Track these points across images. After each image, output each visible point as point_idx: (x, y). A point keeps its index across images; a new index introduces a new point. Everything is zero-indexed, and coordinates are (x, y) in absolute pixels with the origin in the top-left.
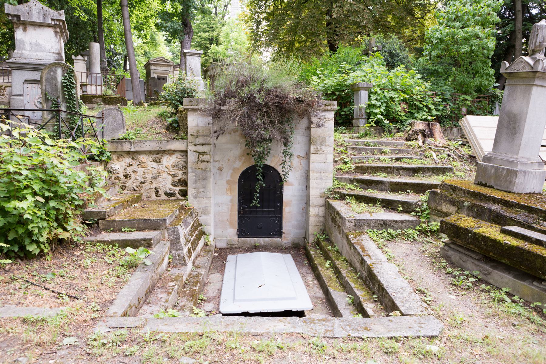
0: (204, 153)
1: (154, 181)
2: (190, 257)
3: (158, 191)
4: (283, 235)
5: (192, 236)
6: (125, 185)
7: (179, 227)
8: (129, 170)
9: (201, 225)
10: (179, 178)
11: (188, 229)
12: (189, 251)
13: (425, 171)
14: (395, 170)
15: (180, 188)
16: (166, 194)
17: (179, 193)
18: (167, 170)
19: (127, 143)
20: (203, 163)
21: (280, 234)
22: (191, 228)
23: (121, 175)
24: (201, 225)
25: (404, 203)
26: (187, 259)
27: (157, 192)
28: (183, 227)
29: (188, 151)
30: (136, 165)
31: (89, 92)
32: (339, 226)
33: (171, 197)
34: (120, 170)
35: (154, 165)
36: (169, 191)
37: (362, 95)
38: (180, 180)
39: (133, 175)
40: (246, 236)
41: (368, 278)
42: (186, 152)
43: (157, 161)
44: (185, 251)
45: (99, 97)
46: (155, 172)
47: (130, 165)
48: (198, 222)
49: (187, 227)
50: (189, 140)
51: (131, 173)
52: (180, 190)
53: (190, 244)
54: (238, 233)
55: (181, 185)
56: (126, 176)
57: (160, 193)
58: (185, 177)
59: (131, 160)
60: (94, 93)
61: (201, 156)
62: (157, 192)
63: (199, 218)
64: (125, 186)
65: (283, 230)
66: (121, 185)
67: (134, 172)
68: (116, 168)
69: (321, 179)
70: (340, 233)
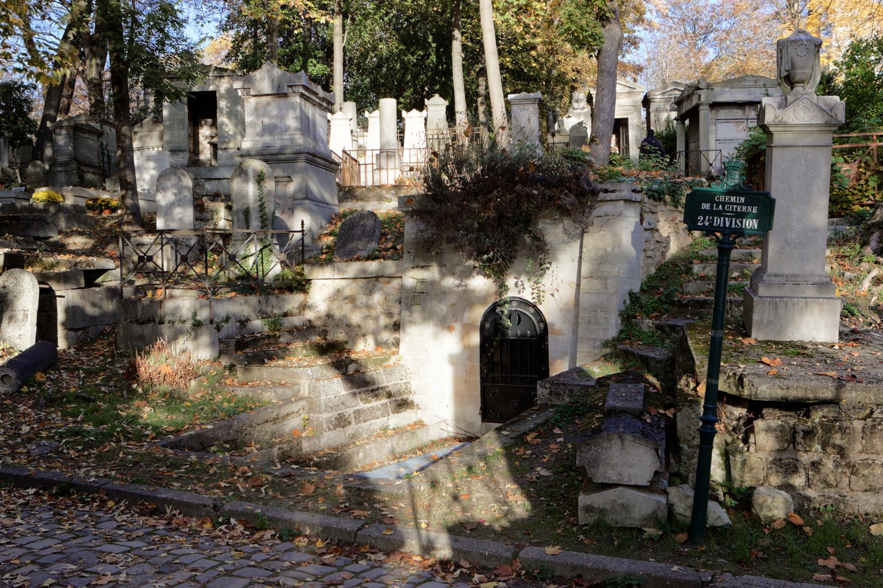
69: (597, 323)
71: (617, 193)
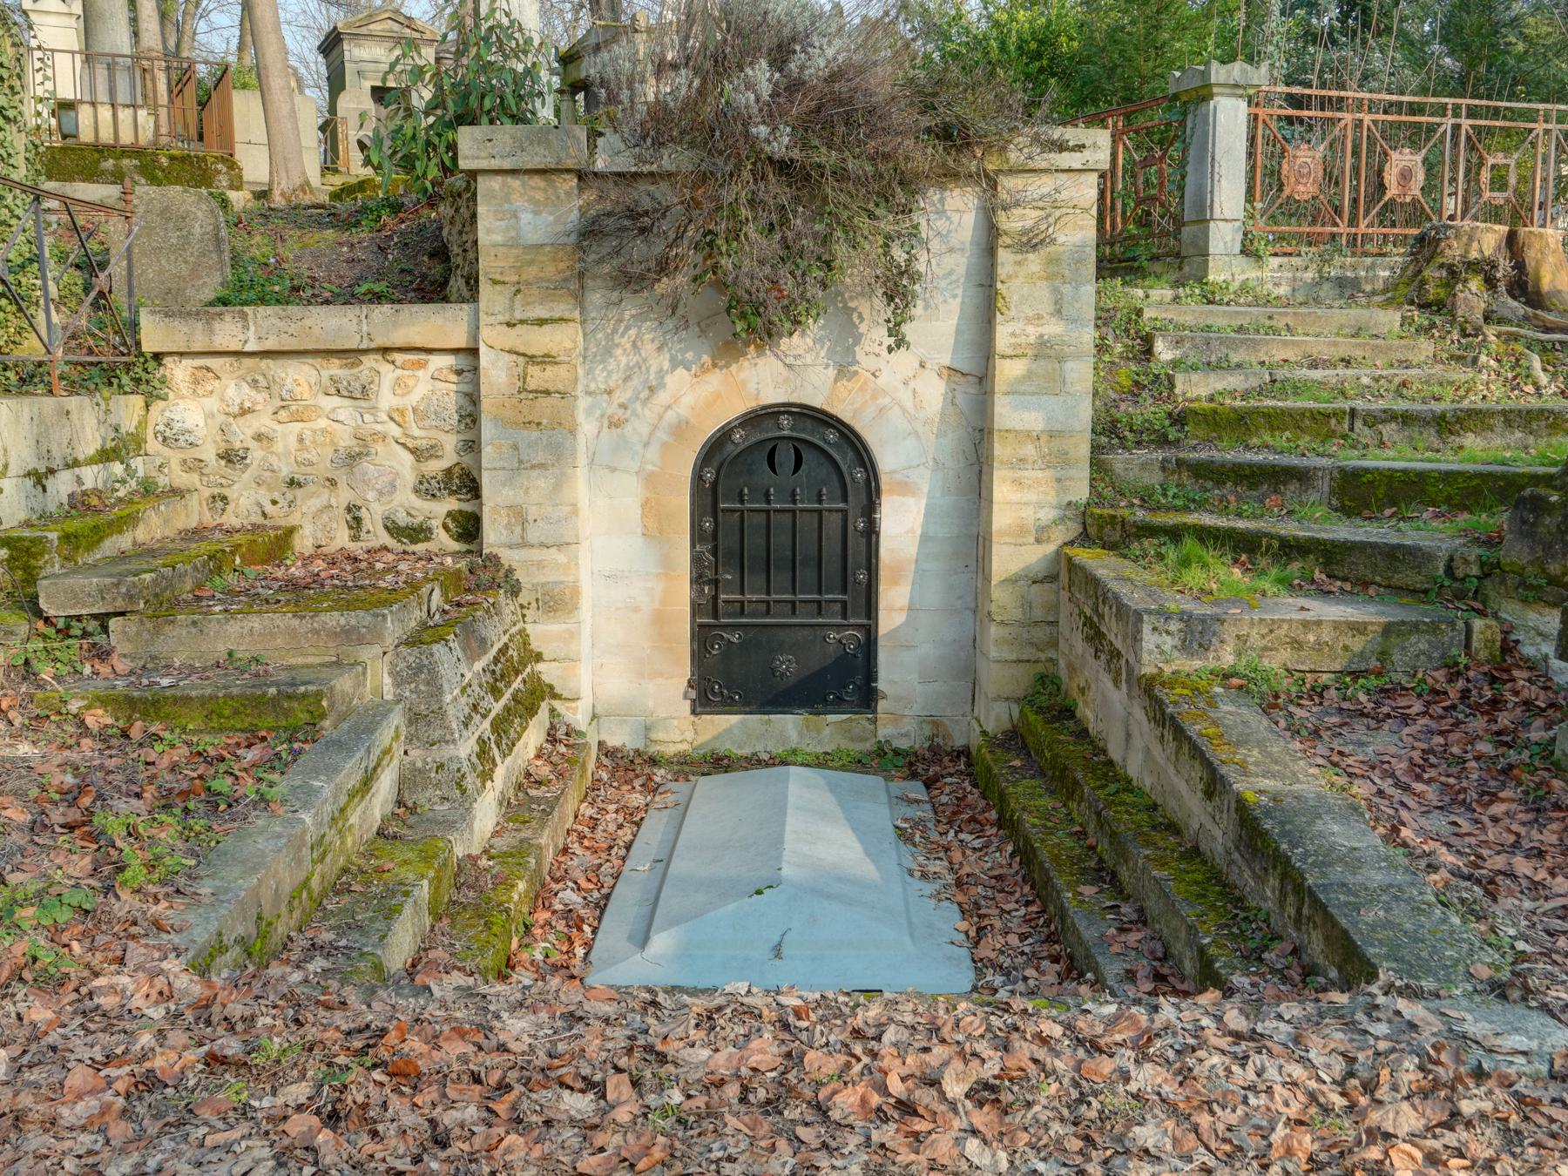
0: (547, 360)
1: (342, 480)
2: (487, 776)
3: (358, 520)
4: (882, 705)
5: (496, 692)
6: (226, 492)
7: (438, 649)
8: (242, 433)
9: (539, 657)
10: (445, 463)
11: (479, 666)
12: (483, 752)
13: (1491, 428)
14: (1358, 424)
15: (451, 504)
16: (394, 529)
17: (445, 527)
18: (395, 431)
19: (228, 318)
20: (544, 401)
21: (867, 698)
22: (496, 660)
23: (209, 453)
24: (539, 657)
25: (1393, 555)
26: (471, 781)
27: (356, 523)
28: (458, 652)
29: (483, 349)
30: (271, 410)
31: (86, 136)
32: (1115, 654)
33: (414, 541)
34: (201, 432)
35: (345, 410)
36: (402, 519)
37: (1221, 118)
38: (448, 472)
39: (257, 454)
40: (726, 705)
41: (1236, 856)
42: (474, 352)
43: (361, 394)
44: (466, 748)
45: (127, 152)
46: (345, 440)
47: (244, 412)
48: (526, 643)
49: (472, 658)
50: (483, 304)
51: (252, 444)
52: (449, 514)
53: (486, 724)
54: (693, 694)
55: (452, 493)
56: (230, 457)
57: (367, 524)
58: (467, 460)
59: (246, 389)
60: (106, 136)
61: (534, 370)
62: (356, 523)
63: (529, 628)
64: (224, 498)
65: (882, 685)
66: (207, 493)
67: (259, 437)
68: (188, 425)
70: (1116, 683)
71: (1087, 154)
